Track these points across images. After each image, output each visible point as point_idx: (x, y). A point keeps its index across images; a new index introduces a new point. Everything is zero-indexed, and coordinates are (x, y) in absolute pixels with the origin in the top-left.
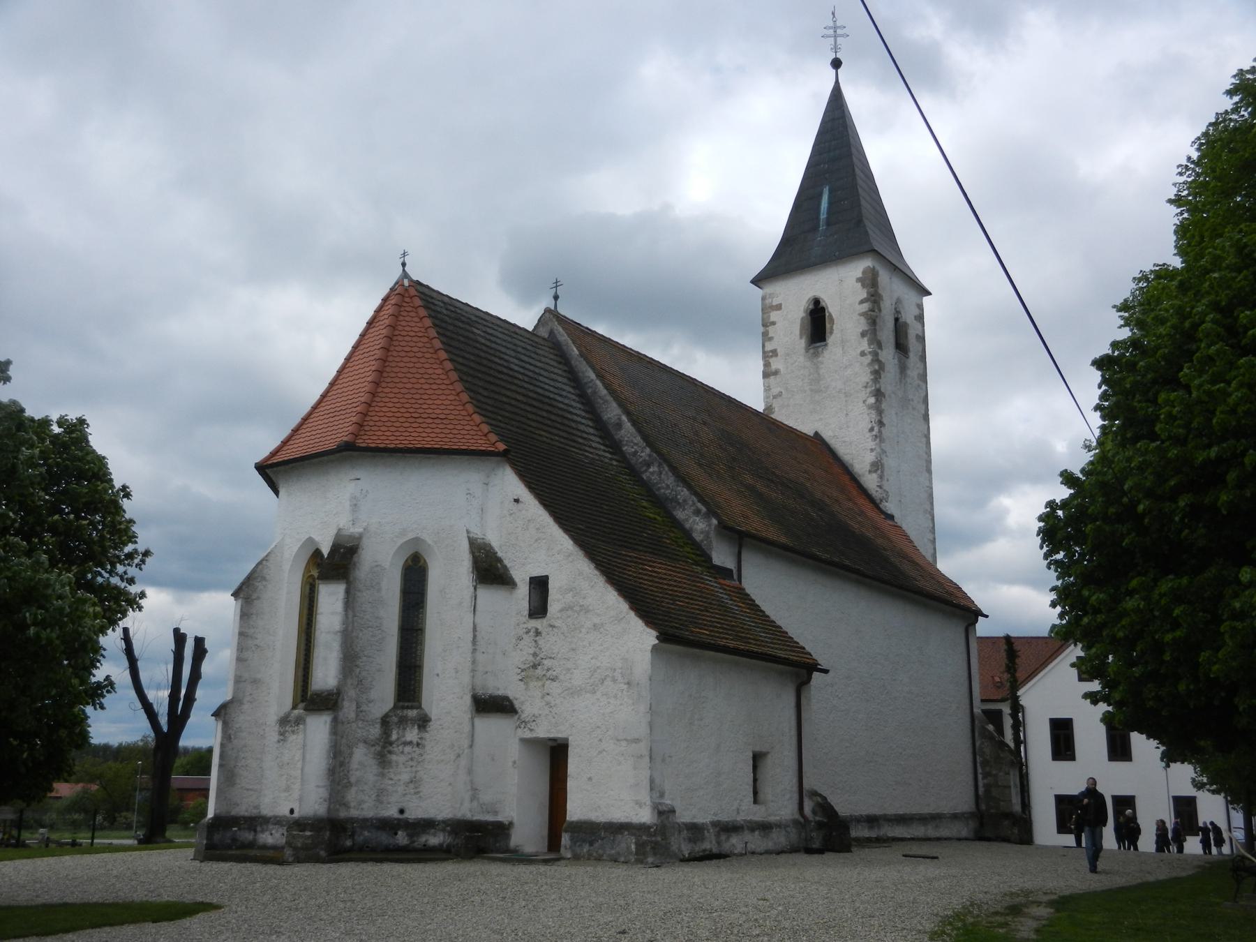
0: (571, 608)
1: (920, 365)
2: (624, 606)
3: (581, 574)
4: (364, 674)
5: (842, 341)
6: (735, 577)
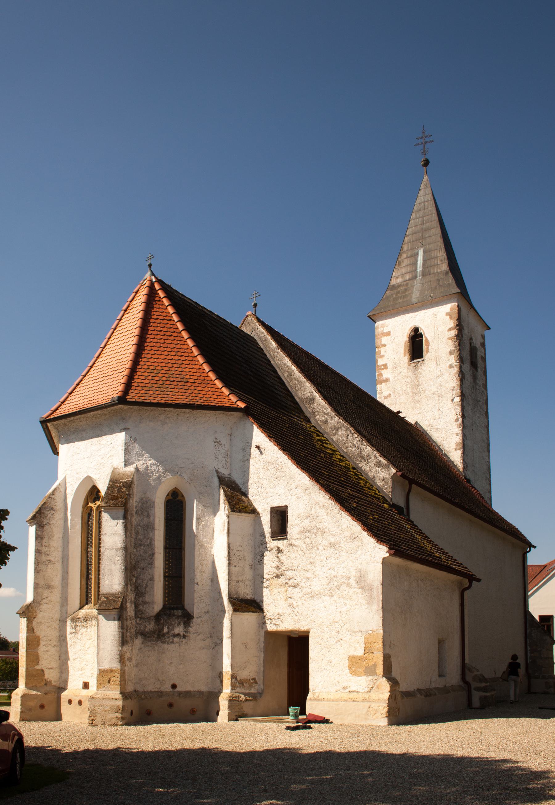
0: (309, 531)
1: (483, 377)
2: (356, 528)
3: (317, 503)
4: (139, 581)
6: (405, 513)
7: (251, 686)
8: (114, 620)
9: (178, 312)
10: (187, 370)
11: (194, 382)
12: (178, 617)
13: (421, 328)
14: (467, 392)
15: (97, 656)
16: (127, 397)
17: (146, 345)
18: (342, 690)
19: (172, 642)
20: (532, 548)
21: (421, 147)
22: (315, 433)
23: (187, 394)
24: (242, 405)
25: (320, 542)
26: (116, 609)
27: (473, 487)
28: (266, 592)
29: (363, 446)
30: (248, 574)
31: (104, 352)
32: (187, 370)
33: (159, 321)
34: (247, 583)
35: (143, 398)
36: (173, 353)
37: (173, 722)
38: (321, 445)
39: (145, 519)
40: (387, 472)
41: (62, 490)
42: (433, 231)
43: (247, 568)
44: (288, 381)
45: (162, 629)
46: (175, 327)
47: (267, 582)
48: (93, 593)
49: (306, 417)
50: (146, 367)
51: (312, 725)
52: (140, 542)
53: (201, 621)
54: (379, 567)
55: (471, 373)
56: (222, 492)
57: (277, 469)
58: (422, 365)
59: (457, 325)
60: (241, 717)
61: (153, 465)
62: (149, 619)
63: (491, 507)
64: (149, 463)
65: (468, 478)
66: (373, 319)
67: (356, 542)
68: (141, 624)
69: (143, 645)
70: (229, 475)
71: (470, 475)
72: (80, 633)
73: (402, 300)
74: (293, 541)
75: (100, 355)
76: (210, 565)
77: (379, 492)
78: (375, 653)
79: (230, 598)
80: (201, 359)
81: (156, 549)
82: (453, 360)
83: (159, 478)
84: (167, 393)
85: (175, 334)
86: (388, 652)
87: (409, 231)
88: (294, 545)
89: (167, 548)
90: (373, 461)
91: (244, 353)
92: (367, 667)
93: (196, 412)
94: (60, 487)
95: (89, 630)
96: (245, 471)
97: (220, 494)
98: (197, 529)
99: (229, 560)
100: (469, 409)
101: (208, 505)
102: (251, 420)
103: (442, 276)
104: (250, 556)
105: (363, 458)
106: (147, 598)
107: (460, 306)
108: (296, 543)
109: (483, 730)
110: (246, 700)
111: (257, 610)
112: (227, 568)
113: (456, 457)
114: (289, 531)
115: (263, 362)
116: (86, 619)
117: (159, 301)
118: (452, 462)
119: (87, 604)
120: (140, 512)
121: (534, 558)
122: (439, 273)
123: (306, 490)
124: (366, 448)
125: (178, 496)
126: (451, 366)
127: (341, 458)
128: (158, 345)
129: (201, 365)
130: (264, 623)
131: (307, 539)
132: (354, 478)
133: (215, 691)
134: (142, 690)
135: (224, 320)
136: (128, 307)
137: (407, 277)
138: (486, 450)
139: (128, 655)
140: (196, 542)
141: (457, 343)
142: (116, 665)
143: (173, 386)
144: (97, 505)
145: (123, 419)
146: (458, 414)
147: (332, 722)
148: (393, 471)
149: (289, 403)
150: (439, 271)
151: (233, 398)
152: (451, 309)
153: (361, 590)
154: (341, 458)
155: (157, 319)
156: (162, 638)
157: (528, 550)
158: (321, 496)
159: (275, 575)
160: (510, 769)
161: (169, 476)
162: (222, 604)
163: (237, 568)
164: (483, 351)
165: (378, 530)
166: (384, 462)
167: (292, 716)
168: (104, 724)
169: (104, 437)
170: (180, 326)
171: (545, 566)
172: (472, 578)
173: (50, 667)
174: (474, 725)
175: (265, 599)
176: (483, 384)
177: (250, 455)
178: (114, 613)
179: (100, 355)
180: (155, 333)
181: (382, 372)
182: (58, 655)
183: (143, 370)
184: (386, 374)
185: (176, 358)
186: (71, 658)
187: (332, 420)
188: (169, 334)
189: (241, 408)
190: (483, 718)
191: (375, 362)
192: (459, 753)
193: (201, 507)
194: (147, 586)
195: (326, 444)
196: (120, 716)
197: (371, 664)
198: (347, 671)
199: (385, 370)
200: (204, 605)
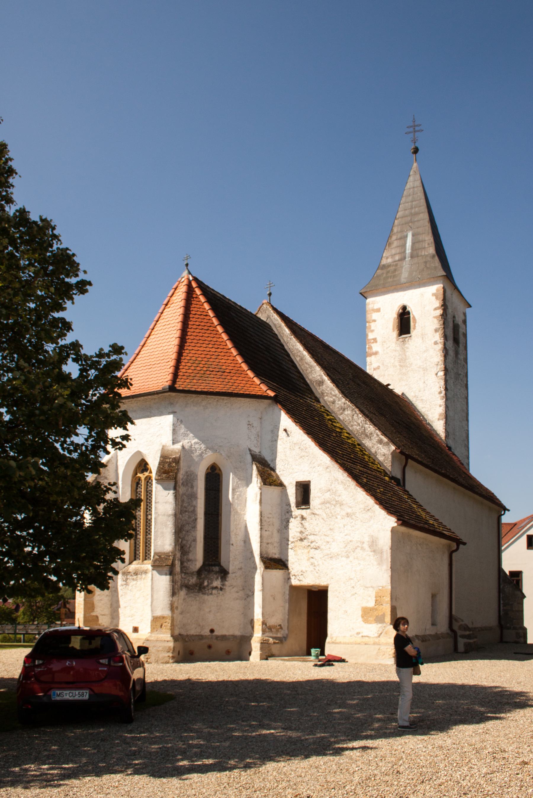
1: (464, 352)
2: (370, 501)
3: (337, 480)
4: (184, 542)
5: (422, 335)
7: (277, 631)
8: (166, 574)
9: (214, 308)
10: (223, 361)
11: (230, 373)
12: (216, 573)
13: (409, 307)
14: (450, 366)
15: (151, 605)
16: (176, 386)
17: (187, 338)
18: (356, 635)
19: (211, 594)
20: (506, 512)
21: (411, 135)
22: (325, 412)
23: (225, 383)
24: (271, 394)
25: (338, 512)
26: (168, 565)
27: (454, 454)
28: (291, 553)
29: (367, 426)
30: (276, 538)
31: (148, 342)
32: (223, 361)
33: (197, 316)
34: (275, 544)
35: (189, 386)
36: (210, 346)
37: (214, 660)
38: (332, 424)
39: (190, 489)
40: (387, 449)
41: (114, 461)
42: (421, 216)
43: (275, 531)
44: (300, 365)
45: (203, 583)
46: (211, 322)
47: (293, 544)
48: (141, 551)
49: (316, 397)
50: (188, 358)
51: (334, 663)
52: (185, 509)
53: (236, 576)
54: (389, 535)
55: (453, 348)
56: (254, 467)
57: (302, 450)
58: (410, 340)
59: (442, 306)
60: (270, 657)
61: (197, 443)
62: (192, 574)
63: (469, 471)
64: (193, 442)
65: (449, 445)
66: (364, 295)
67: (369, 514)
68: (185, 578)
69: (186, 596)
70: (260, 452)
71: (451, 443)
72: (130, 585)
73: (392, 280)
74: (315, 510)
75: (145, 344)
76: (243, 529)
77: (380, 466)
78: (384, 605)
79: (262, 558)
80: (234, 352)
81: (198, 515)
82: (438, 337)
83: (201, 455)
84: (208, 382)
85: (211, 328)
86: (394, 604)
87: (399, 214)
88: (316, 514)
89: (206, 514)
90: (375, 439)
91: (264, 341)
92: (377, 616)
93: (232, 399)
94: (112, 459)
95: (139, 582)
96: (273, 450)
97: (252, 469)
98: (233, 498)
99: (261, 525)
100: (451, 382)
101: (242, 478)
102: (280, 406)
103: (429, 259)
104: (278, 522)
105: (367, 436)
106: (191, 556)
107: (446, 287)
108: (317, 513)
109: (473, 668)
110: (274, 643)
111: (283, 567)
112: (259, 532)
113: (439, 427)
114: (312, 502)
115: (278, 347)
116: (136, 574)
117: (196, 298)
118: (436, 431)
119: (135, 560)
120: (185, 483)
121: (506, 519)
122: (427, 256)
123: (327, 468)
124: (369, 427)
125: (215, 469)
126: (436, 343)
127: (348, 435)
128: (198, 338)
129: (235, 357)
130: (289, 578)
131: (328, 510)
132: (360, 454)
133: (247, 635)
134: (185, 634)
135: (245, 310)
136: (169, 301)
137: (397, 258)
138: (465, 419)
139: (176, 605)
140: (232, 509)
141: (442, 322)
142: (167, 613)
143: (212, 376)
144: (145, 476)
145: (172, 404)
146: (442, 387)
147: (347, 662)
148: (393, 448)
149: (302, 385)
150: (426, 253)
151: (264, 387)
152: (437, 290)
153: (373, 553)
154: (348, 435)
155: (195, 314)
156: (203, 590)
157: (503, 513)
158: (340, 474)
159: (299, 538)
160: (501, 691)
161: (210, 453)
162: (254, 562)
163: (267, 532)
164: (465, 328)
165: (387, 503)
166: (385, 440)
167: (314, 656)
168: (157, 662)
169: (153, 418)
170: (215, 321)
171: (515, 524)
172: (459, 542)
173: (103, 613)
174: (464, 665)
175: (290, 558)
176: (464, 358)
177: (278, 437)
178: (166, 569)
179: (145, 344)
180: (195, 327)
181: (372, 345)
182: (110, 603)
183: (186, 361)
184: (375, 347)
185: (213, 350)
186: (121, 606)
187: (339, 401)
188: (206, 328)
189: (271, 397)
190: (470, 660)
191: (365, 336)
192: (459, 682)
193: (236, 480)
194: (190, 546)
195: (335, 422)
196: (171, 655)
197: (381, 614)
198: (360, 619)
199: (375, 344)
200: (238, 562)
